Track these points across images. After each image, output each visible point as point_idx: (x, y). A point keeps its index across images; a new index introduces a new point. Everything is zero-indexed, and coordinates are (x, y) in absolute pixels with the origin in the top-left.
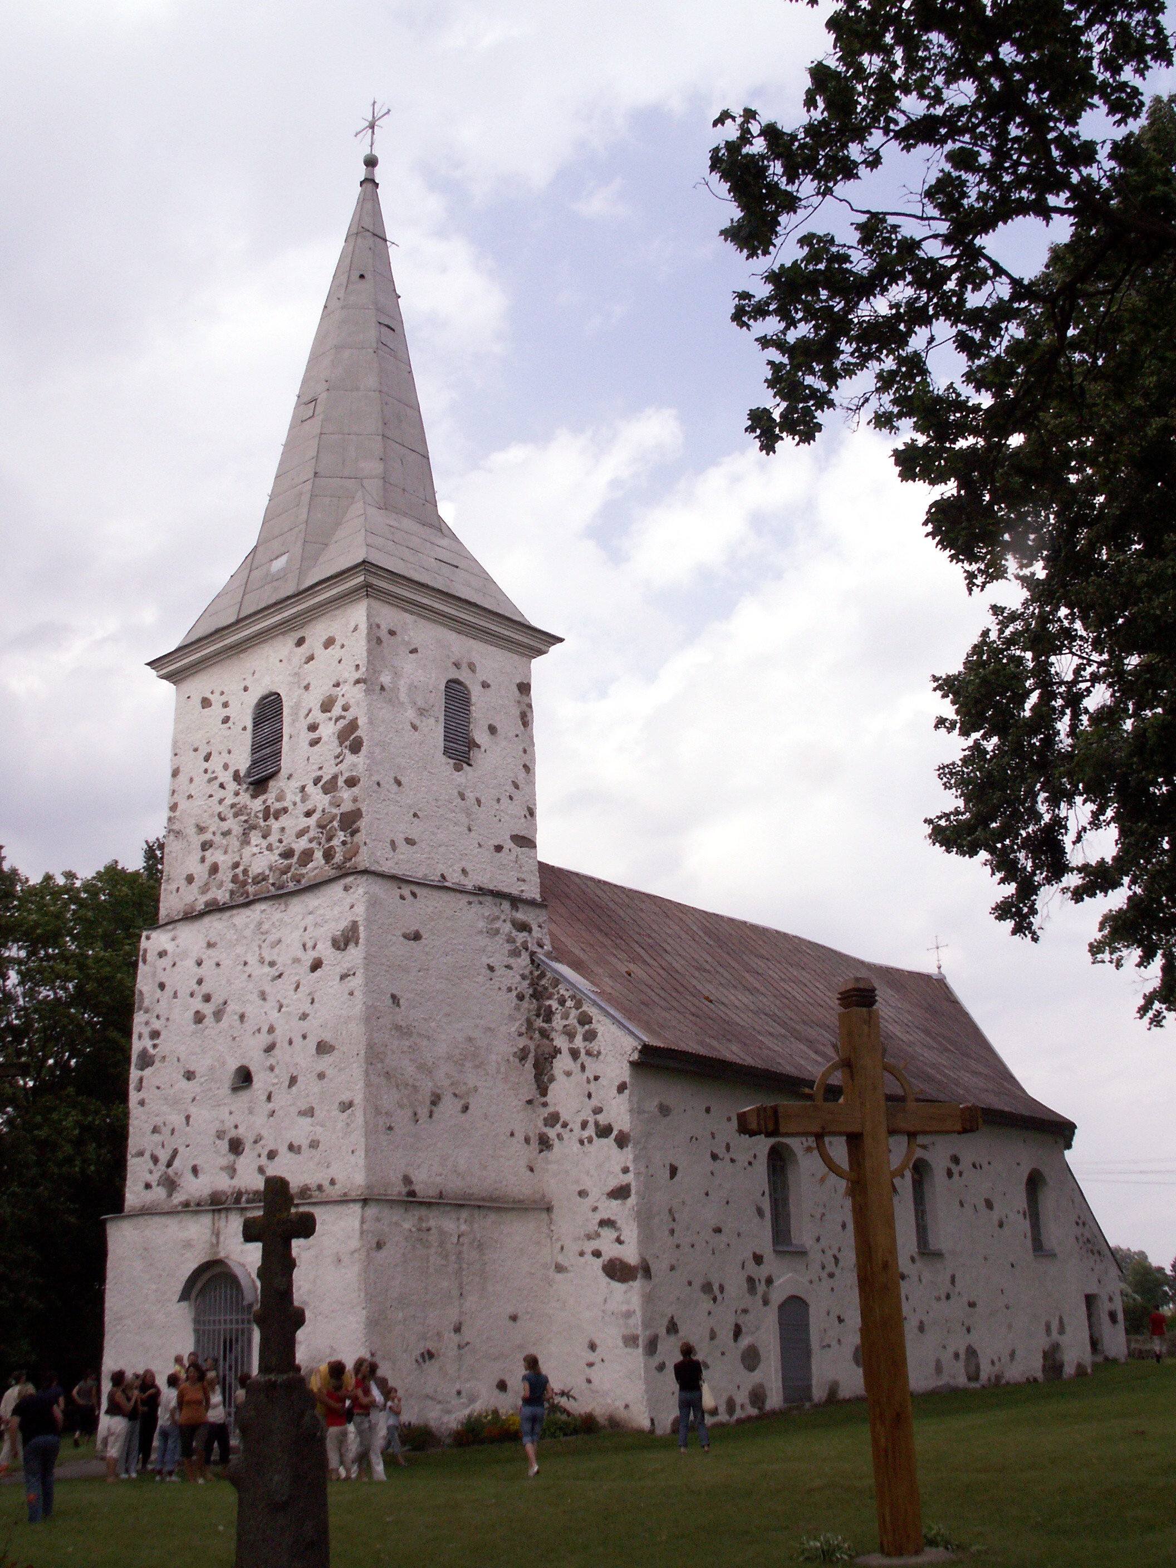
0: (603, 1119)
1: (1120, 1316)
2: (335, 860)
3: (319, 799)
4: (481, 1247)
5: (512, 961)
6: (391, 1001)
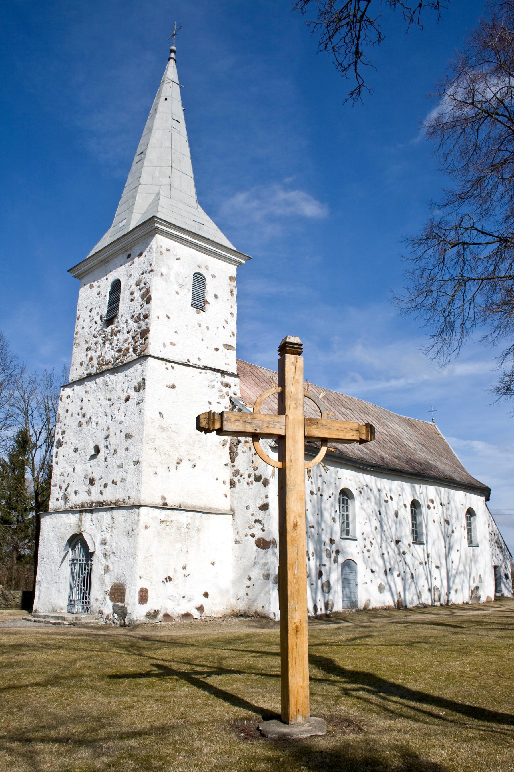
0: (258, 473)
1: (510, 576)
2: (138, 352)
3: (133, 325)
4: (198, 530)
5: (220, 400)
6: (159, 415)
